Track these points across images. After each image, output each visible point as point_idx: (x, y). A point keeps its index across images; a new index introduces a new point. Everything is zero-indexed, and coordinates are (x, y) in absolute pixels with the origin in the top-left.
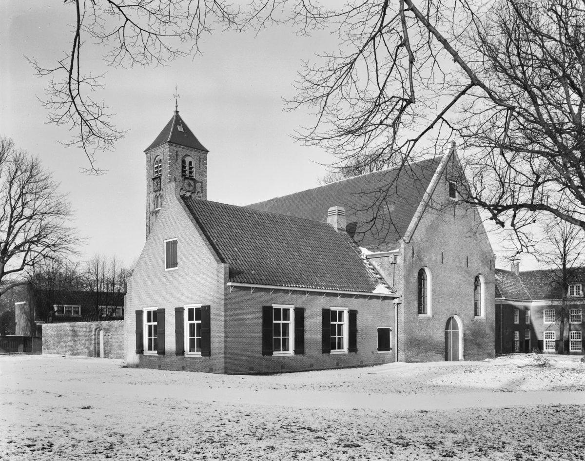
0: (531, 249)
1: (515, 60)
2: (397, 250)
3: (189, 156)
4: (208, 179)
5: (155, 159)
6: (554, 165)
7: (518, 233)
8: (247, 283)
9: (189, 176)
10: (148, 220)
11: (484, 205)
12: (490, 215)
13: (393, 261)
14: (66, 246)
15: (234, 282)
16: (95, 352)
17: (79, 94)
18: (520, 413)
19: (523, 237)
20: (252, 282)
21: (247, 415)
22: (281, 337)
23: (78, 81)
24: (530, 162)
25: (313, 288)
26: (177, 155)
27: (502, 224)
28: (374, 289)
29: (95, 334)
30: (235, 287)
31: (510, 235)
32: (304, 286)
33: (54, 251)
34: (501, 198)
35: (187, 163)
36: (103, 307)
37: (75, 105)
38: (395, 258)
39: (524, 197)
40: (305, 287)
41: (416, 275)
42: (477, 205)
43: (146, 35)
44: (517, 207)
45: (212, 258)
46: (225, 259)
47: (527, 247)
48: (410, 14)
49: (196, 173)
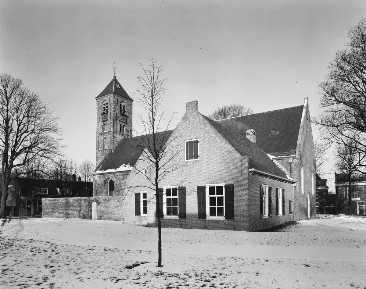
3: (124, 102)
4: (133, 116)
5: (103, 103)
10: (98, 138)
16: (89, 216)
26: (117, 101)
35: (122, 106)
36: (65, 189)
49: (127, 113)
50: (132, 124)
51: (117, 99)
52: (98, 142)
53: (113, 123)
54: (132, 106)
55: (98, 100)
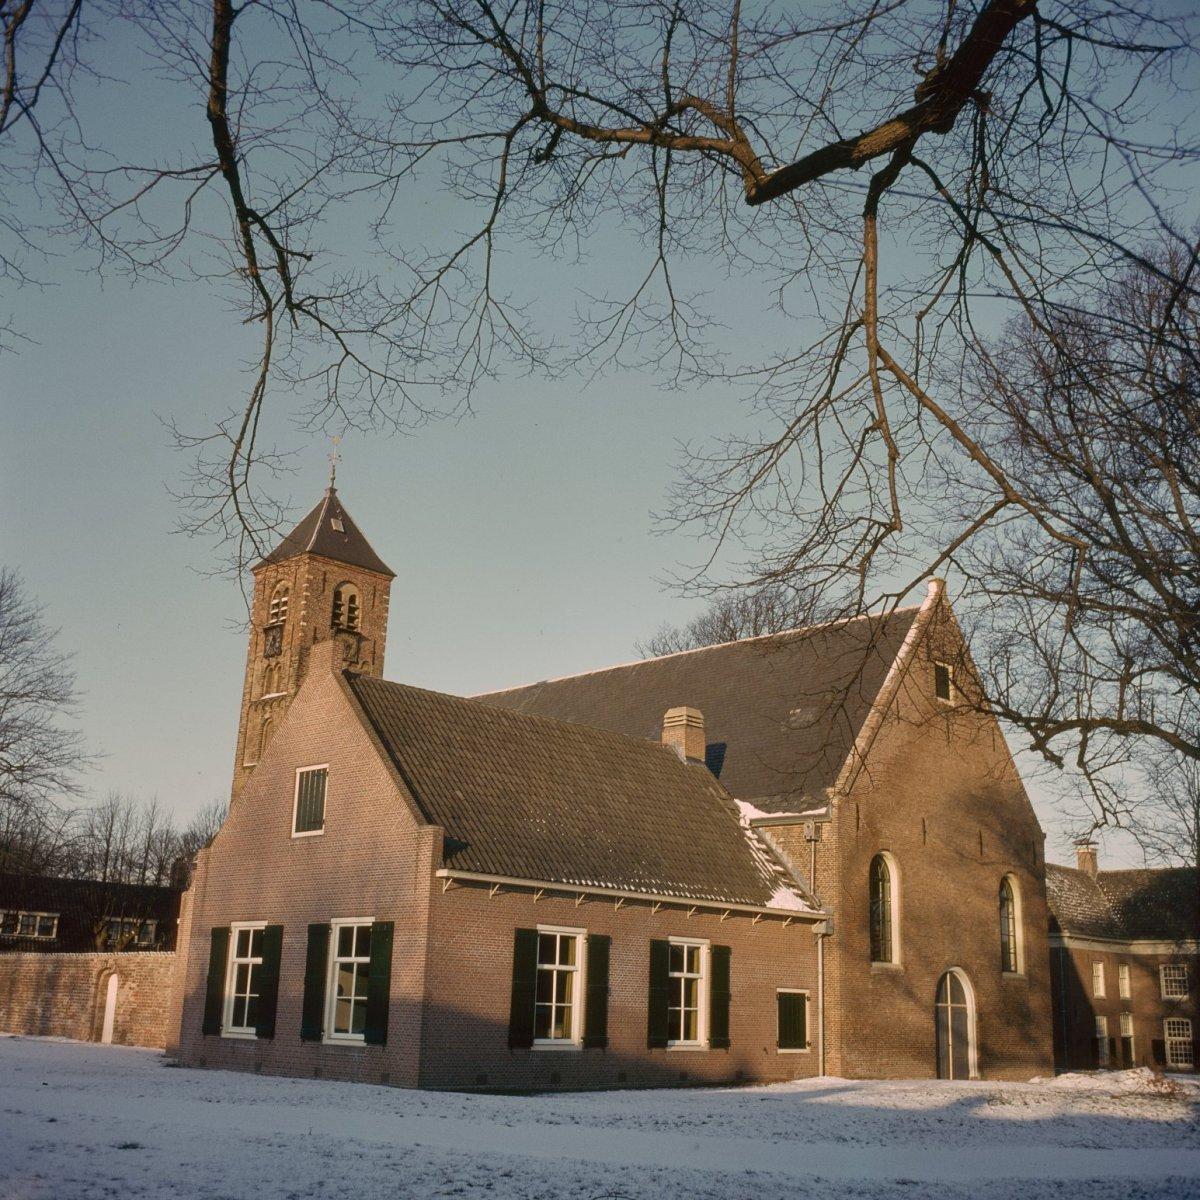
0: (1124, 820)
1: (1066, 424)
2: (823, 811)
4: (389, 635)
5: (274, 587)
6: (1159, 636)
7: (1095, 783)
8: (484, 872)
9: (348, 627)
10: (244, 722)
11: (1015, 717)
12: (1031, 740)
13: (813, 834)
14: (49, 770)
15: (453, 868)
17: (245, 482)
18: (1129, 1191)
19: (1107, 792)
20: (494, 871)
21: (506, 1175)
23: (248, 460)
24: (1110, 630)
25: (630, 890)
26: (324, 580)
27: (1057, 761)
28: (770, 898)
29: (97, 984)
30: (456, 880)
31: (1078, 785)
32: (610, 885)
33: (22, 781)
34: (1051, 702)
35: (345, 598)
37: (236, 503)
38: (818, 829)
39: (1104, 699)
40: (613, 888)
41: (866, 869)
42: (1002, 718)
43: (378, 380)
44: (1087, 725)
45: (405, 811)
46: (435, 816)
47: (1108, 816)
48: (888, 375)
50: (382, 666)
51: (325, 573)
52: (243, 733)
53: (296, 665)
54: (388, 594)
55: (260, 577)
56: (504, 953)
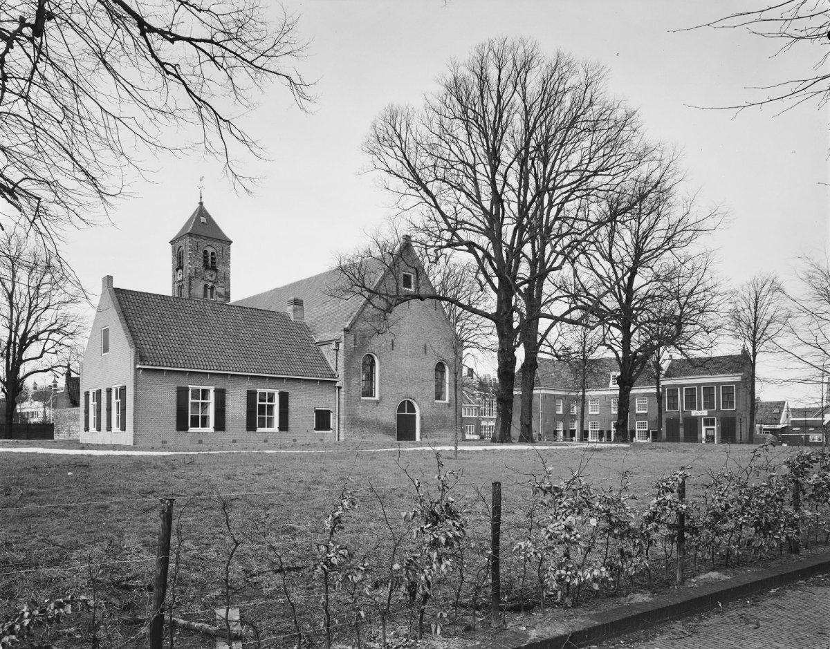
4: (231, 269)
22: (266, 416)
54: (229, 250)
56: (173, 396)
